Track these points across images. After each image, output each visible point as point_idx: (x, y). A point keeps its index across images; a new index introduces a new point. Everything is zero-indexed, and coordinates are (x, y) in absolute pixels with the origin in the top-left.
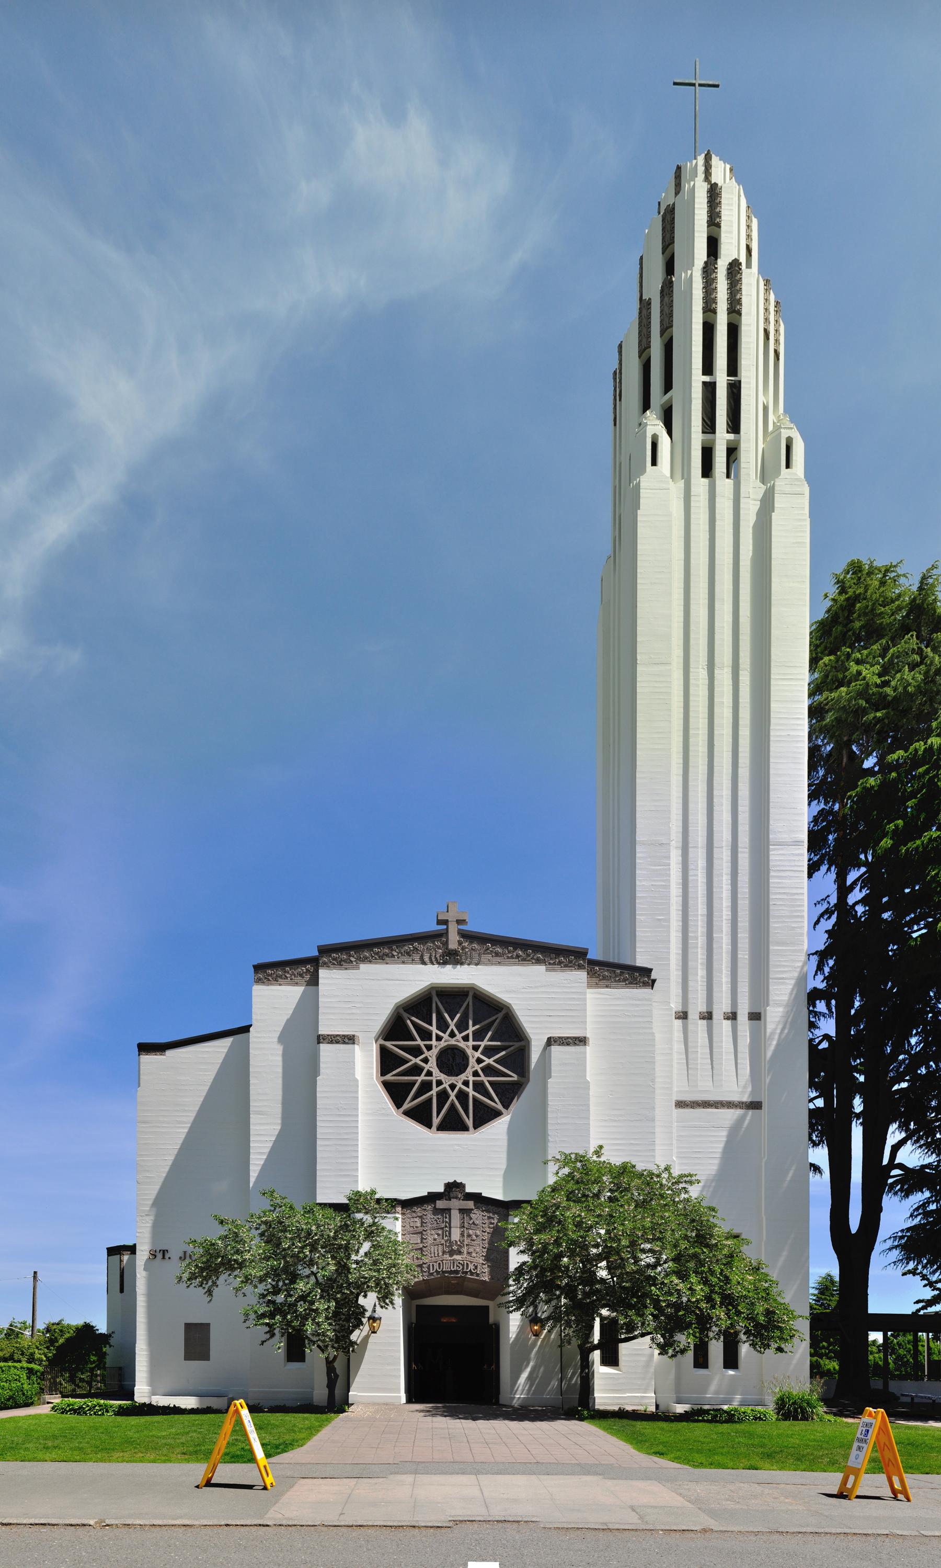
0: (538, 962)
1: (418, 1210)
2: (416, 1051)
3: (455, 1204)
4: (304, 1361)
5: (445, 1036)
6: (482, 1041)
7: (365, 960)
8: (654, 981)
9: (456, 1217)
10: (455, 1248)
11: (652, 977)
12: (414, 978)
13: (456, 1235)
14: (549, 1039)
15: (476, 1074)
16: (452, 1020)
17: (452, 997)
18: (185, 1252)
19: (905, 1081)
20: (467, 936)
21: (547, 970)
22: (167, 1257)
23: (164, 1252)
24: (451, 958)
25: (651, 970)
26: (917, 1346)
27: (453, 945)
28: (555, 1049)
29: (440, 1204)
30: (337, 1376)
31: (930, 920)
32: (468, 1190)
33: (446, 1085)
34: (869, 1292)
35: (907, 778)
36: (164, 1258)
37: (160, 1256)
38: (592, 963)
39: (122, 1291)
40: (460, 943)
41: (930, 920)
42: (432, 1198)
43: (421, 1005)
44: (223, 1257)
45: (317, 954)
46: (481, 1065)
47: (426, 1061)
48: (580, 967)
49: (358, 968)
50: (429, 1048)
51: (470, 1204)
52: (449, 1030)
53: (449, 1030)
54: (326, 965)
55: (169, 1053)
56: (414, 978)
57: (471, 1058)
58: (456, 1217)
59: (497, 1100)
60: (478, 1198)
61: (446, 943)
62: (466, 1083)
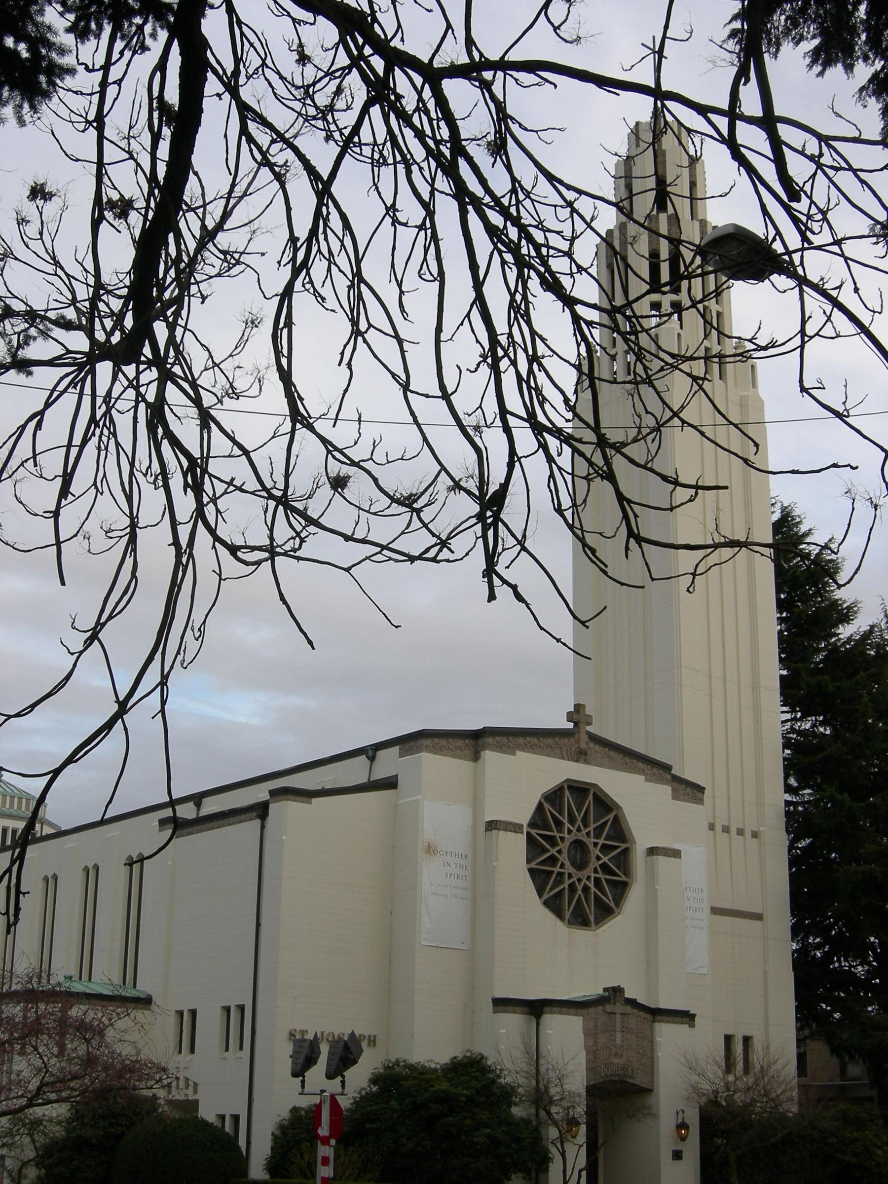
0: (639, 771)
1: (592, 1010)
9: (618, 1017)
12: (556, 771)
17: (579, 790)
19: (821, 661)
20: (595, 739)
24: (581, 756)
26: (686, 357)
27: (583, 746)
31: (842, 995)
34: (203, 106)
35: (803, 18)
40: (587, 744)
41: (842, 995)
46: (572, 828)
49: (514, 754)
51: (629, 1009)
55: (315, 800)
56: (556, 771)
58: (618, 1017)
60: (632, 1003)
61: (578, 742)
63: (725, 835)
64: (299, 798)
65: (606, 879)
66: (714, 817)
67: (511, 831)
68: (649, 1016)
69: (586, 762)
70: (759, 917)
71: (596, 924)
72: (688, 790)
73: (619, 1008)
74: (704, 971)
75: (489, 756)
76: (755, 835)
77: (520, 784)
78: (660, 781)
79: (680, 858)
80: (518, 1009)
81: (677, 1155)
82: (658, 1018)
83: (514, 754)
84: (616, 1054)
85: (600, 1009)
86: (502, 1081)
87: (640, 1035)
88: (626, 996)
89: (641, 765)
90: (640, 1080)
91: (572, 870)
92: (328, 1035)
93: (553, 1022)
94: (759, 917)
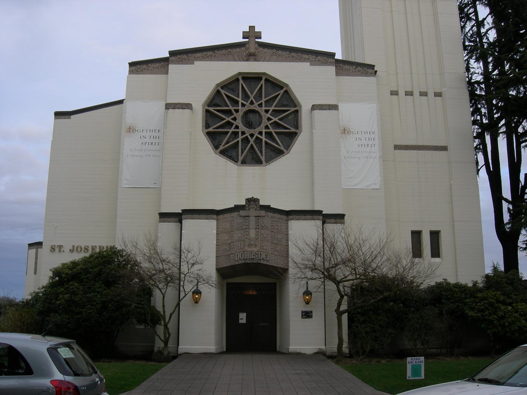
0: (305, 60)
2: (228, 112)
3: (253, 212)
4: (432, 257)
5: (256, 135)
6: (271, 107)
7: (199, 59)
8: (376, 72)
9: (252, 220)
10: (252, 243)
11: (375, 70)
13: (252, 233)
14: (313, 106)
15: (267, 127)
16: (252, 94)
18: (73, 246)
21: (311, 65)
22: (62, 250)
23: (60, 247)
24: (251, 57)
25: (374, 66)
27: (252, 50)
28: (317, 112)
29: (242, 213)
30: (169, 334)
32: (261, 203)
33: (247, 134)
36: (60, 251)
37: (57, 250)
38: (338, 61)
39: (35, 273)
40: (257, 49)
42: (237, 208)
43: (231, 84)
44: (346, 295)
45: (168, 56)
47: (235, 119)
48: (331, 64)
49: (193, 64)
50: (237, 111)
51: (263, 213)
52: (250, 101)
53: (250, 101)
54: (174, 63)
55: (72, 117)
57: (263, 118)
58: (252, 220)
59: (280, 144)
60: (268, 208)
62: (260, 133)
63: (424, 98)
64: (62, 117)
65: (275, 132)
66: (398, 86)
67: (179, 108)
68: (284, 217)
69: (256, 60)
70: (444, 148)
71: (266, 162)
72: (359, 68)
73: (253, 212)
74: (377, 187)
75: (172, 68)
76: (438, 95)
77: (201, 82)
78: (326, 64)
79: (338, 110)
80: (173, 219)
81: (307, 315)
82: (290, 217)
83: (193, 64)
84: (250, 245)
85: (235, 214)
86: (421, 287)
87: (275, 231)
88: (261, 204)
89: (306, 56)
90: (274, 261)
91: (244, 129)
92: (77, 247)
93: (190, 225)
94: (444, 148)
